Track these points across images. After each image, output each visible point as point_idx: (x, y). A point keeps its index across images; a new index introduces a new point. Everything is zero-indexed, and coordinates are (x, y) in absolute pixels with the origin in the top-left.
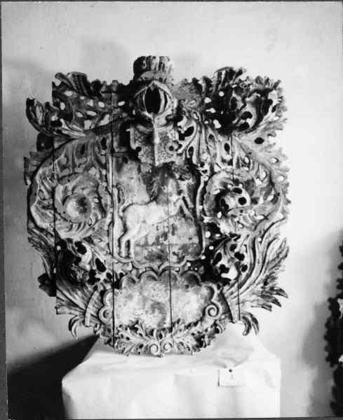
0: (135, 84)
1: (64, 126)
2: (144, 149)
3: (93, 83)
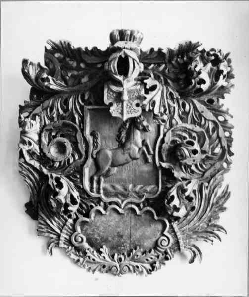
0: (113, 50)
1: (52, 82)
2: (115, 105)
3: (31, 97)
